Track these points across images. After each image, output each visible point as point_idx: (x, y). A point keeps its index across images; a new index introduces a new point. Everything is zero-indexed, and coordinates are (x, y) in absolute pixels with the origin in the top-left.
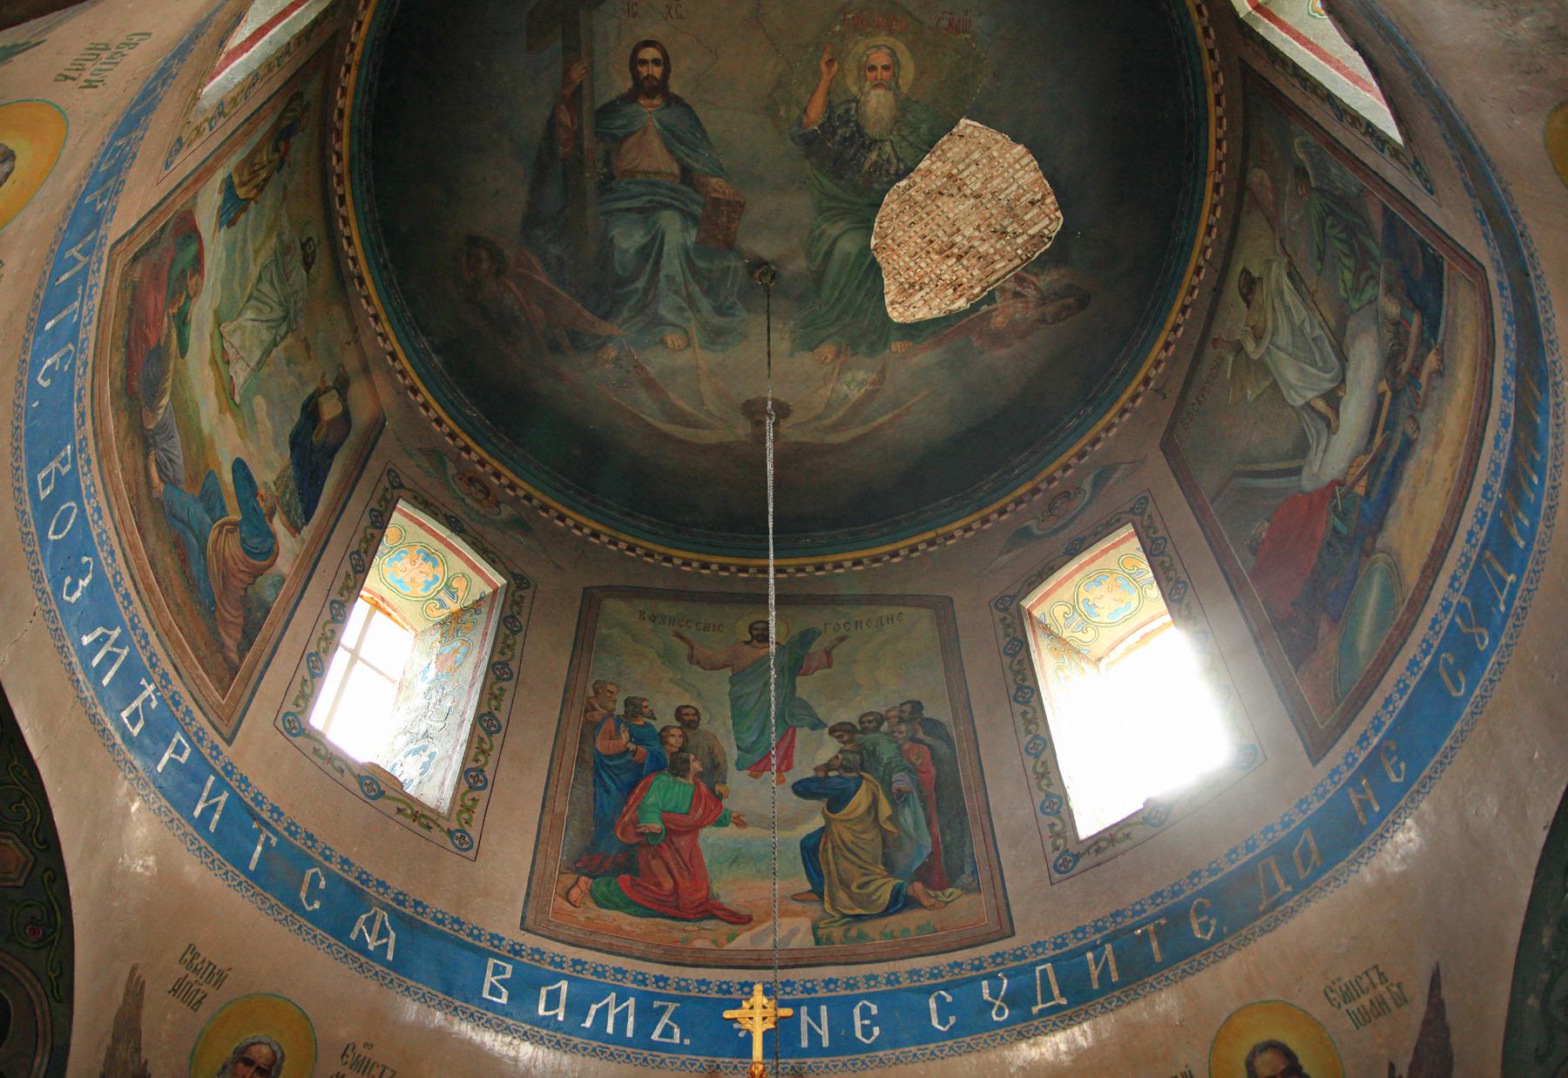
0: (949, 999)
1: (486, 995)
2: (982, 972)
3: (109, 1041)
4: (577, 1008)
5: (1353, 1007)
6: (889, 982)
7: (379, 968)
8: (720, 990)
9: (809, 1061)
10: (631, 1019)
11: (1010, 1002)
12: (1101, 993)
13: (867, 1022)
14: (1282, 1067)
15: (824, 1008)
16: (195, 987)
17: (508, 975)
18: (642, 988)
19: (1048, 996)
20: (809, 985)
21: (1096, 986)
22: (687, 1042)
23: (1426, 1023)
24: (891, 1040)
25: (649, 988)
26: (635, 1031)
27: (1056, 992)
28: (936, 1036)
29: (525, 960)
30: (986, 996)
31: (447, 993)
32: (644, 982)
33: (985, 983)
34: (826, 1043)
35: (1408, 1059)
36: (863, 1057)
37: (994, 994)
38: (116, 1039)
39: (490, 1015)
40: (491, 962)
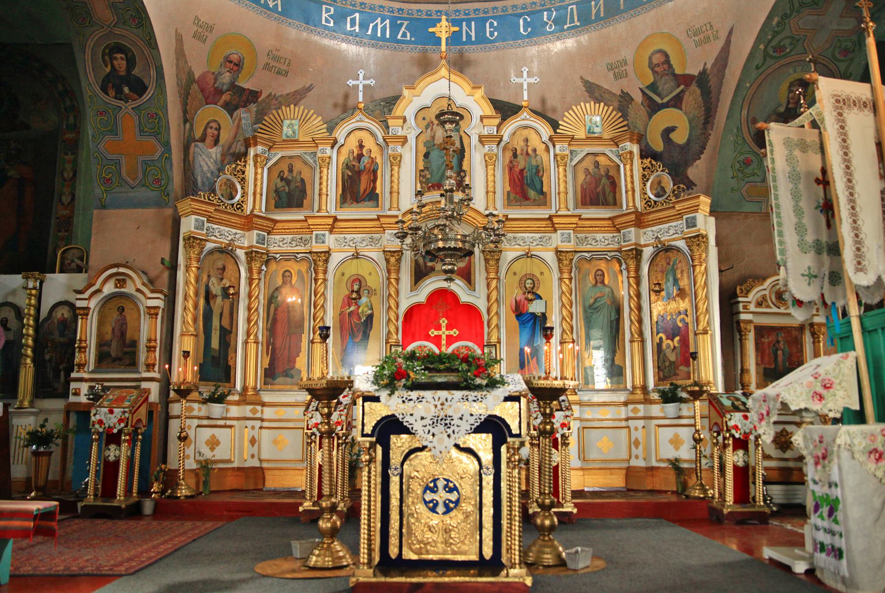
0: (529, 20)
1: (323, 23)
2: (545, 7)
3: (175, 61)
4: (364, 26)
5: (696, 39)
6: (503, 11)
7: (276, 15)
8: (427, 15)
9: (466, 47)
10: (388, 30)
11: (555, 22)
12: (595, 21)
13: (492, 30)
14: (663, 60)
15: (473, 23)
16: (202, 34)
17: (332, 12)
18: (392, 14)
19: (572, 21)
20: (467, 12)
21: (593, 18)
22: (413, 39)
23: (723, 48)
24: (502, 38)
25: (395, 15)
26: (390, 35)
27: (576, 19)
28: (523, 37)
29: (339, 4)
30: (545, 19)
31: (307, 23)
32: (392, 12)
33: (545, 13)
34: (473, 39)
35: (712, 62)
36: (489, 45)
37: (549, 19)
38: (177, 60)
39: (327, 32)
40: (324, 7)
